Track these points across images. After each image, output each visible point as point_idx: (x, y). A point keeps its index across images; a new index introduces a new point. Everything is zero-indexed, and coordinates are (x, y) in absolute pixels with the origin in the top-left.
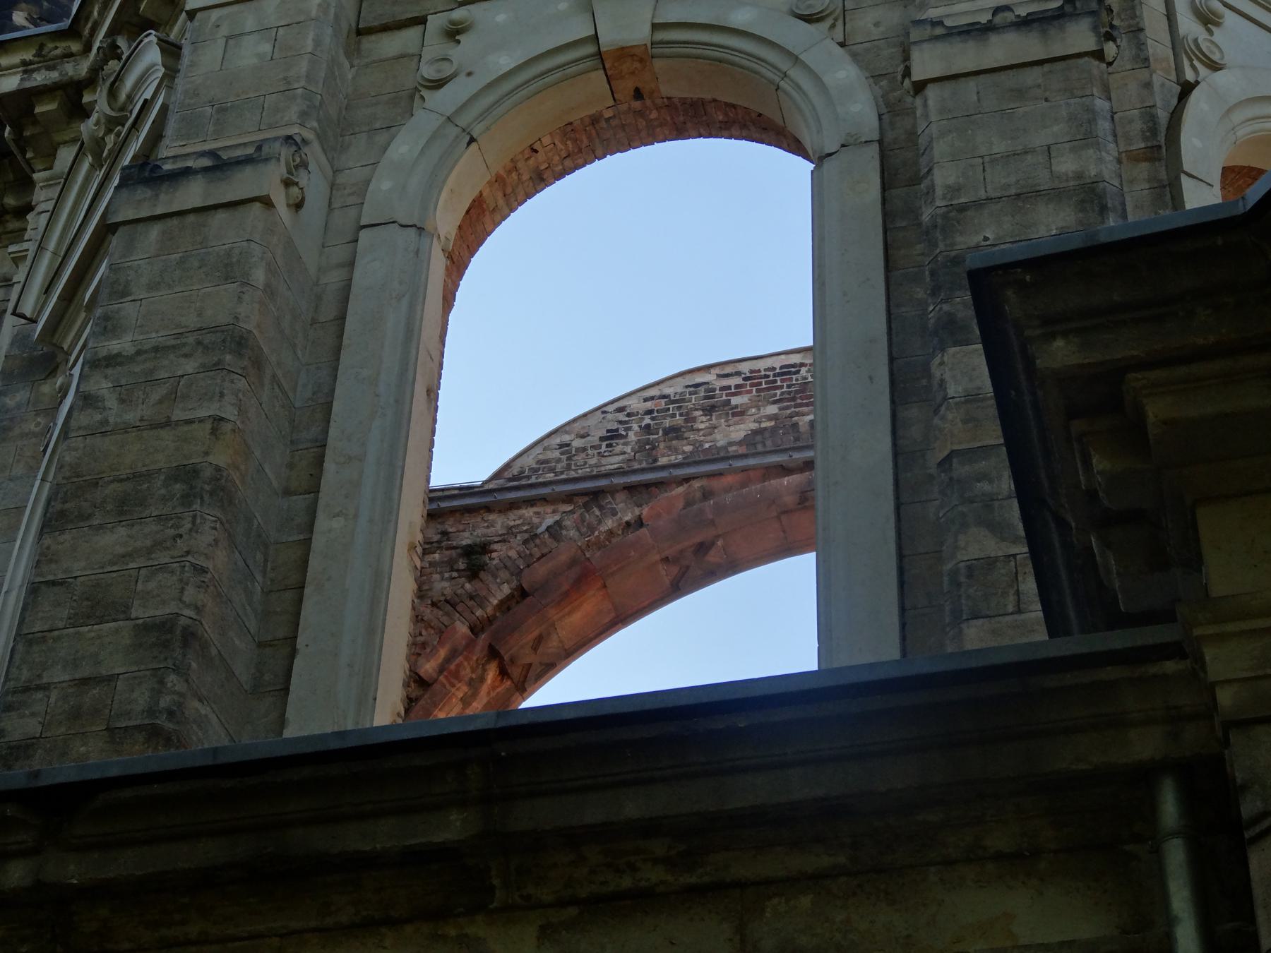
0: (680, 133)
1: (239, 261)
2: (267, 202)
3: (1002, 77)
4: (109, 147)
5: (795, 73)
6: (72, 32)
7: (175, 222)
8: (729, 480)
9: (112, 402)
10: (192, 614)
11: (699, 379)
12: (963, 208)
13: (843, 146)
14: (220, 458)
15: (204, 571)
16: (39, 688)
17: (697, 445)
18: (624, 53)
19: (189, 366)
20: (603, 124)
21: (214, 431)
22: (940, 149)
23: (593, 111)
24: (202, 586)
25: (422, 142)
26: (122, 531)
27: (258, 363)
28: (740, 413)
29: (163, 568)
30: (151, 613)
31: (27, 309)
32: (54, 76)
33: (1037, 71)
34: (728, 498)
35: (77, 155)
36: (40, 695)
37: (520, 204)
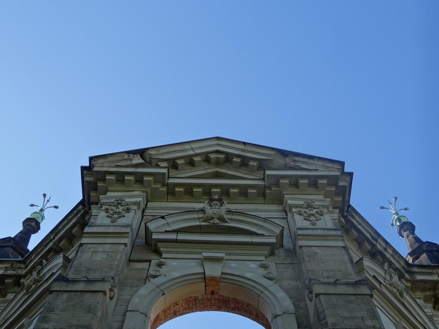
0: (219, 309)
1: (93, 308)
3: (343, 296)
4: (32, 288)
5: (266, 292)
7: (73, 293)
13: (284, 313)
18: (213, 279)
20: (198, 301)
22: (327, 312)
23: (197, 295)
25: (149, 291)
32: (14, 272)
33: (353, 297)
35: (14, 297)
37: (168, 321)
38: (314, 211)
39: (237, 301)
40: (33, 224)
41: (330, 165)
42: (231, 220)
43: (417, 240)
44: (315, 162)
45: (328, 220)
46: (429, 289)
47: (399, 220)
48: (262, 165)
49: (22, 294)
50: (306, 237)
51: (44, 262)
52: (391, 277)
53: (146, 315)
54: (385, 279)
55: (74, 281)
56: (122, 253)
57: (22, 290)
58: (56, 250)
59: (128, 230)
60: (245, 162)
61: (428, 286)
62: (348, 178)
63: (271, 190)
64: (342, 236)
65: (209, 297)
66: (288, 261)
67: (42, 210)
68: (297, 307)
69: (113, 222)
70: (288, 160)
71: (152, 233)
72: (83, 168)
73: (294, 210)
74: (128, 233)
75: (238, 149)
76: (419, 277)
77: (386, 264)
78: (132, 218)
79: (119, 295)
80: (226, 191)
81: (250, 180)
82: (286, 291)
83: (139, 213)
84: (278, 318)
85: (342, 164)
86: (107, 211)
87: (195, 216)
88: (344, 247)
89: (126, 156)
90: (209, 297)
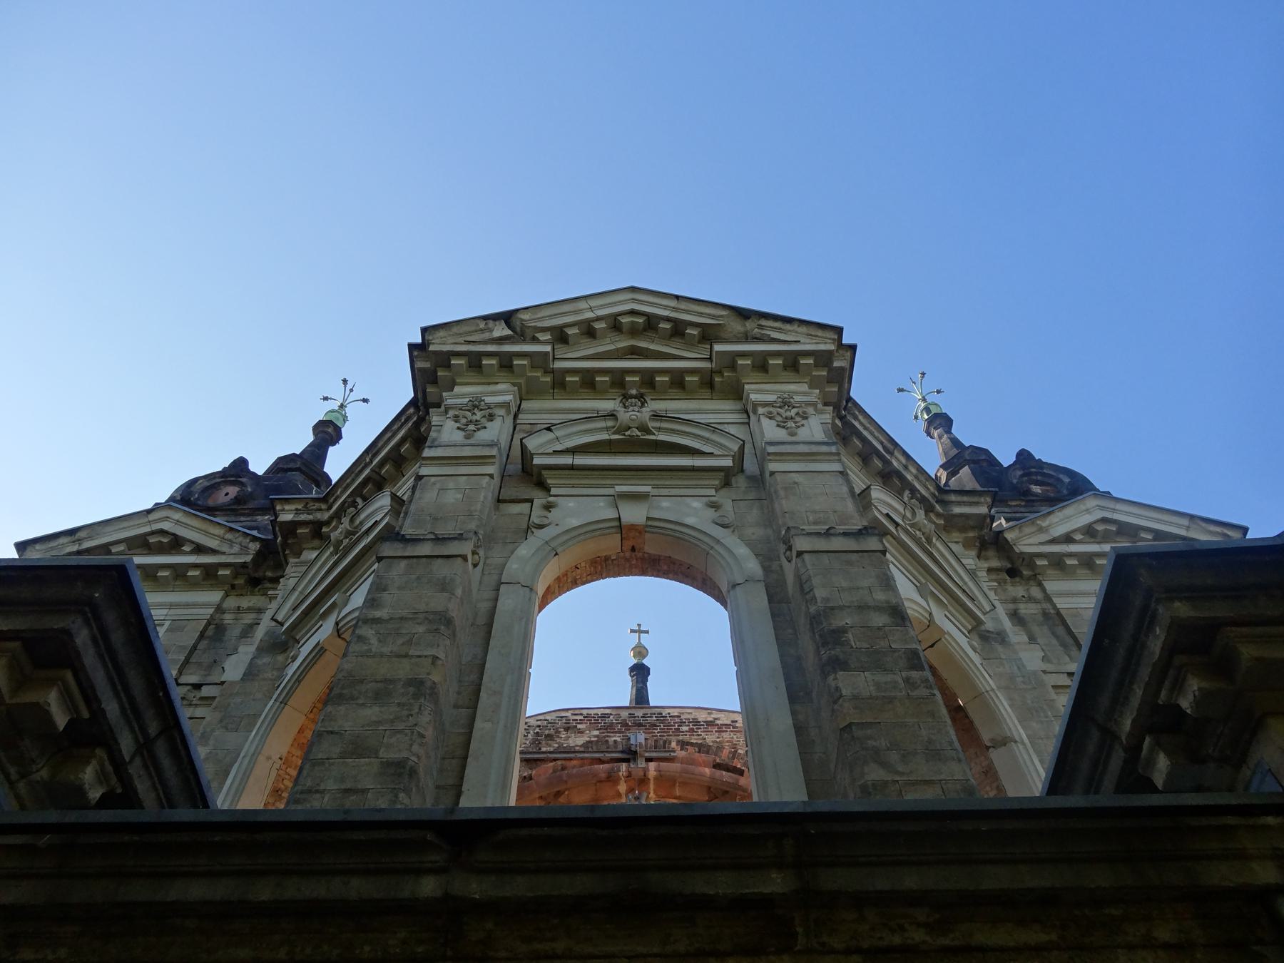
0: (643, 573)
2: (465, 558)
5: (717, 547)
6: (324, 500)
8: (574, 762)
9: (374, 641)
10: (415, 759)
11: (563, 714)
12: (832, 608)
14: (436, 677)
15: (423, 736)
16: (317, 791)
17: (561, 745)
18: (633, 527)
19: (421, 629)
21: (433, 663)
22: (816, 581)
24: (421, 745)
26: (376, 709)
27: (454, 635)
28: (581, 732)
29: (399, 732)
30: (392, 756)
31: (280, 618)
32: (311, 517)
34: (575, 771)
36: (318, 796)
38: (794, 411)
39: (671, 561)
40: (330, 430)
41: (820, 333)
42: (659, 429)
43: (956, 442)
44: (795, 327)
45: (816, 427)
46: (973, 528)
47: (927, 409)
48: (708, 335)
49: (328, 553)
50: (781, 456)
51: (359, 500)
52: (914, 514)
53: (531, 589)
54: (904, 517)
55: (415, 540)
56: (487, 490)
57: (327, 547)
58: (377, 483)
59: (494, 452)
60: (678, 330)
61: (971, 523)
62: (848, 354)
63: (723, 376)
64: (838, 454)
65: (628, 554)
66: (752, 496)
67: (342, 406)
68: (767, 570)
69: (467, 437)
70: (750, 325)
71: (532, 455)
72: (412, 347)
73: (761, 410)
74: (493, 457)
75: (666, 307)
76: (957, 510)
77: (907, 493)
78: (497, 430)
79: (486, 558)
80: (648, 379)
81: (690, 360)
82: (750, 544)
83: (509, 421)
84: (738, 588)
85: (839, 331)
86: (456, 419)
87: (601, 424)
88: (841, 472)
89: (482, 325)
90: (628, 554)
